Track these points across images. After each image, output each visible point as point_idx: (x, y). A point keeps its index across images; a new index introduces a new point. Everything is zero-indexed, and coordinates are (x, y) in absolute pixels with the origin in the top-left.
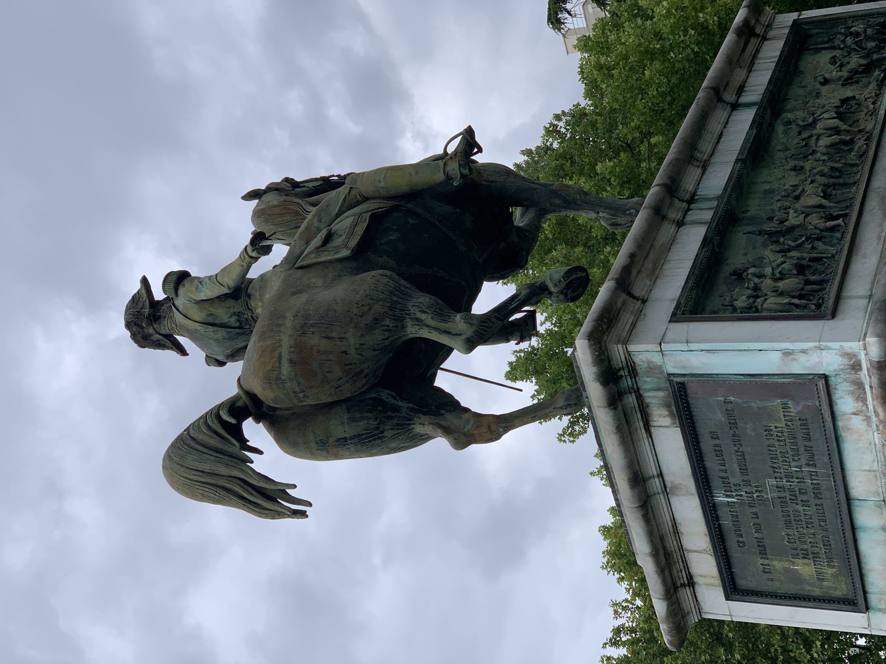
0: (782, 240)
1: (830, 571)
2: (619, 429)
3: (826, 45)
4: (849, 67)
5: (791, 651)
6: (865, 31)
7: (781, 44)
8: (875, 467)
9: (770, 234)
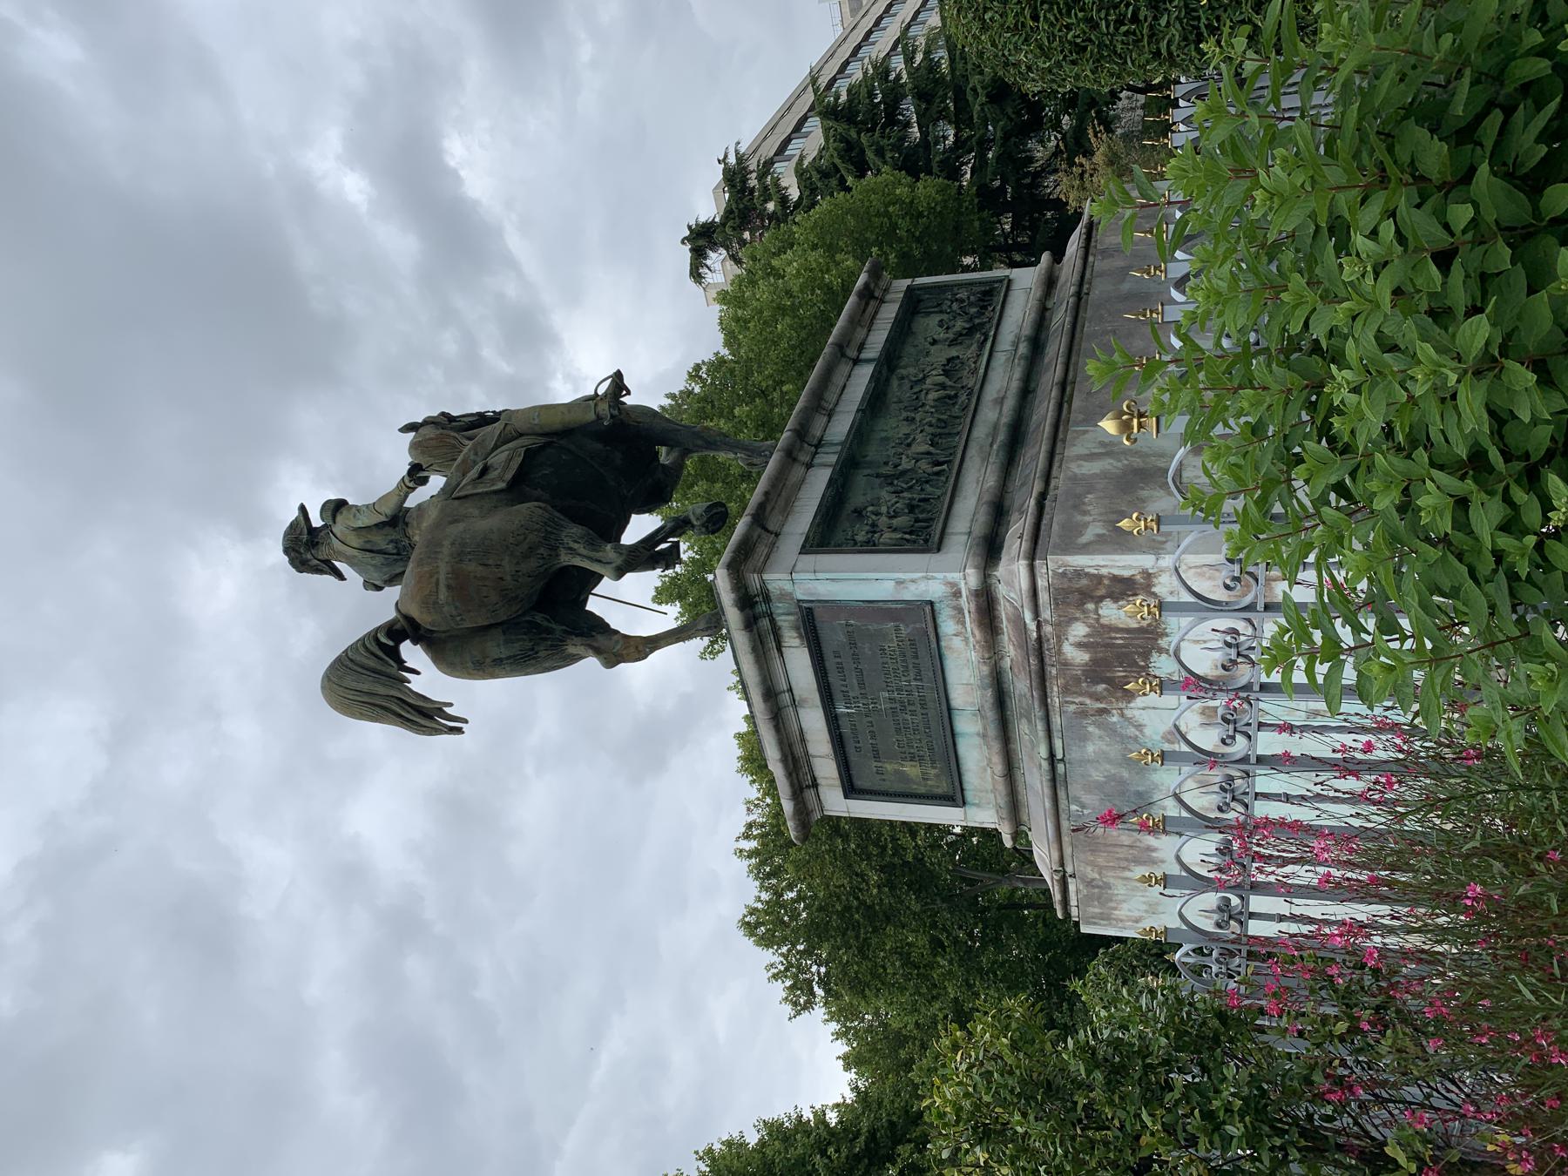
1: (933, 772)
2: (754, 650)
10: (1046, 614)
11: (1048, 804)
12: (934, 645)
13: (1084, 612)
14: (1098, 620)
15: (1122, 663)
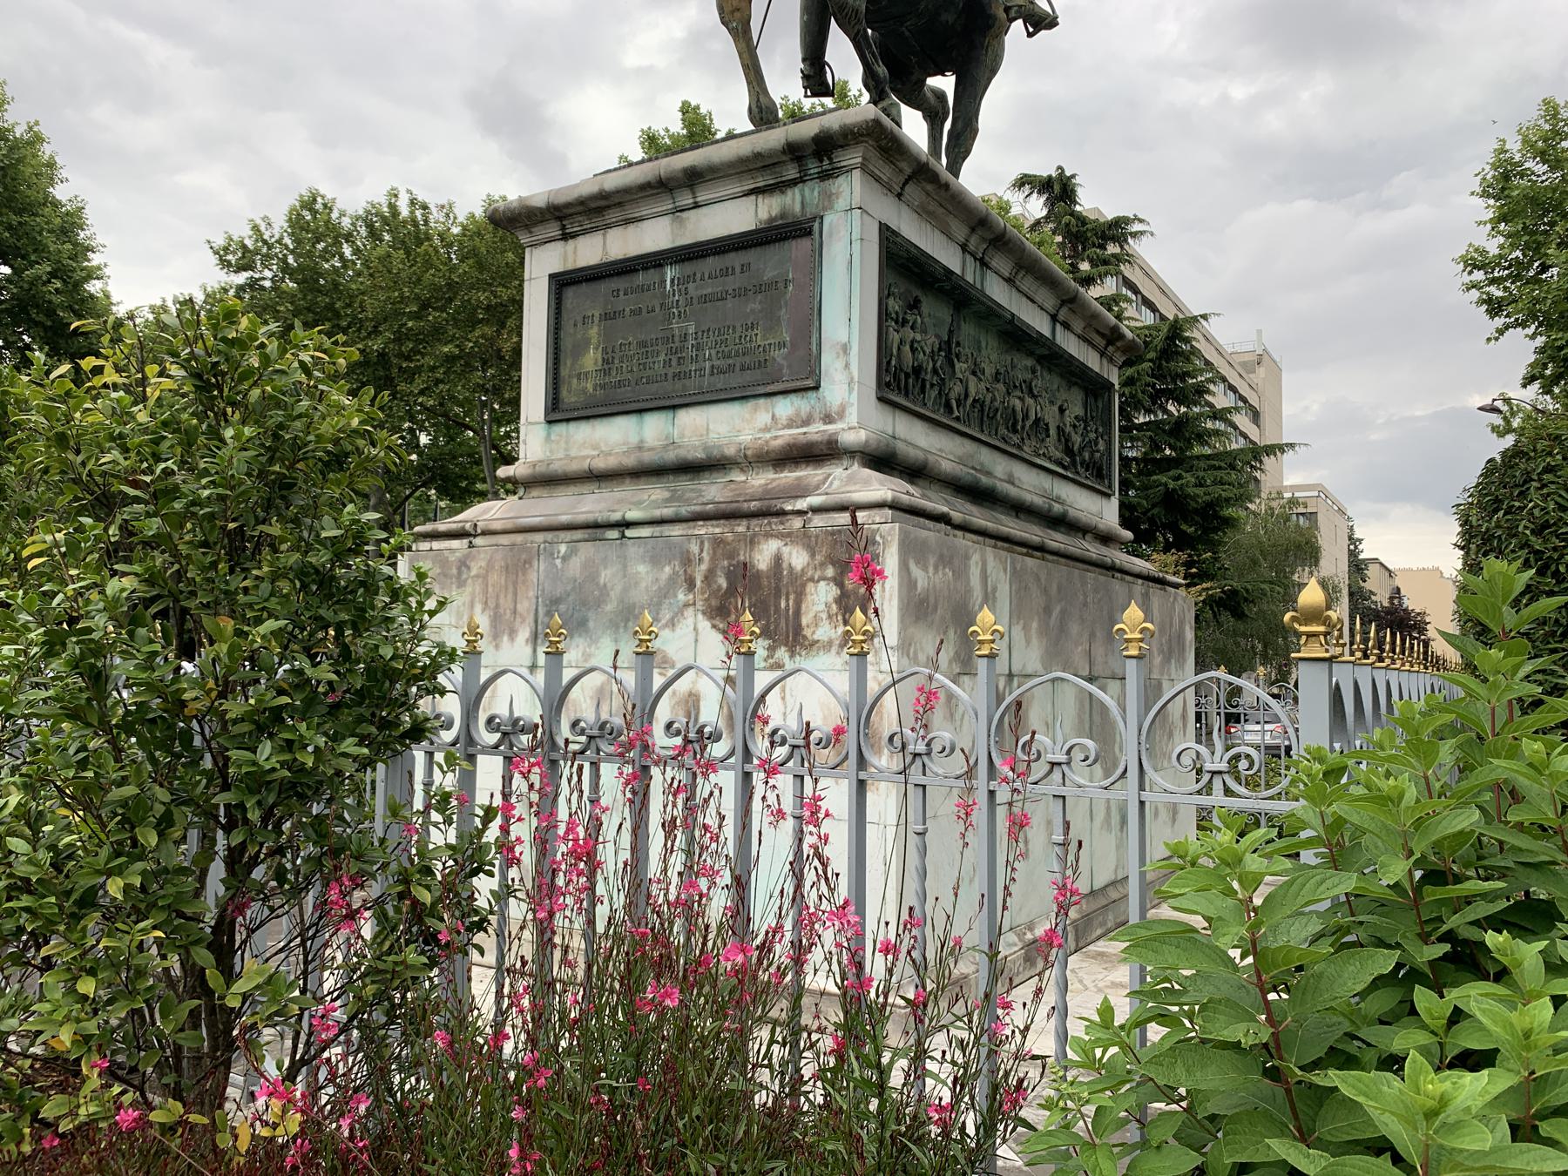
1: (590, 387)
2: (758, 156)
8: (712, 435)
9: (949, 343)
10: (818, 521)
11: (564, 519)
12: (762, 390)
13: (822, 565)
14: (812, 579)
15: (753, 607)
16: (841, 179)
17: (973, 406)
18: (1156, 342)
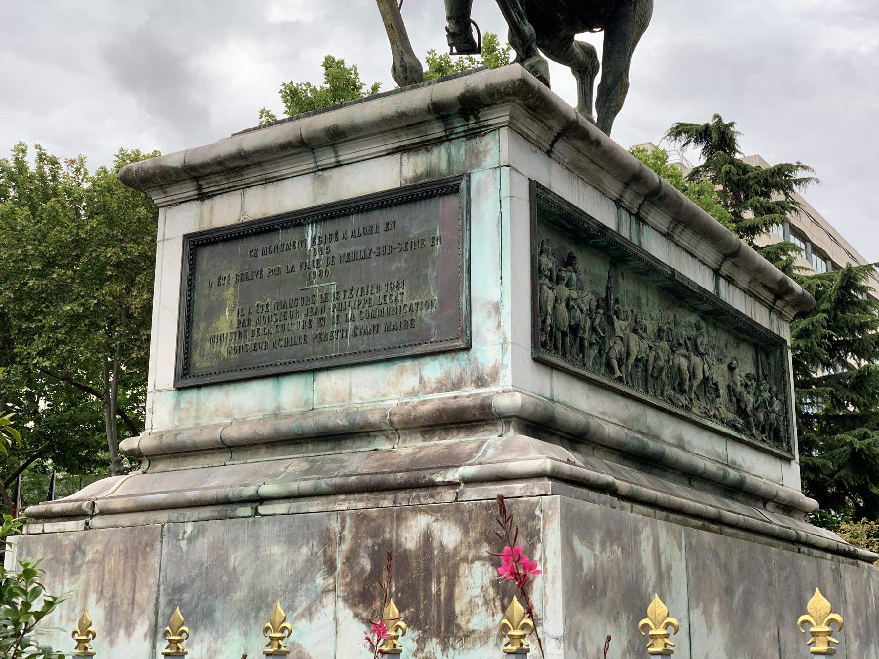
0: (601, 311)
1: (224, 350)
2: (402, 115)
3: (761, 372)
4: (745, 393)
5: (39, 336)
6: (773, 412)
7: (766, 325)
8: (355, 400)
9: (607, 299)
10: (471, 493)
12: (408, 352)
13: (477, 542)
14: (465, 560)
16: (488, 138)
17: (636, 366)
18: (829, 291)
